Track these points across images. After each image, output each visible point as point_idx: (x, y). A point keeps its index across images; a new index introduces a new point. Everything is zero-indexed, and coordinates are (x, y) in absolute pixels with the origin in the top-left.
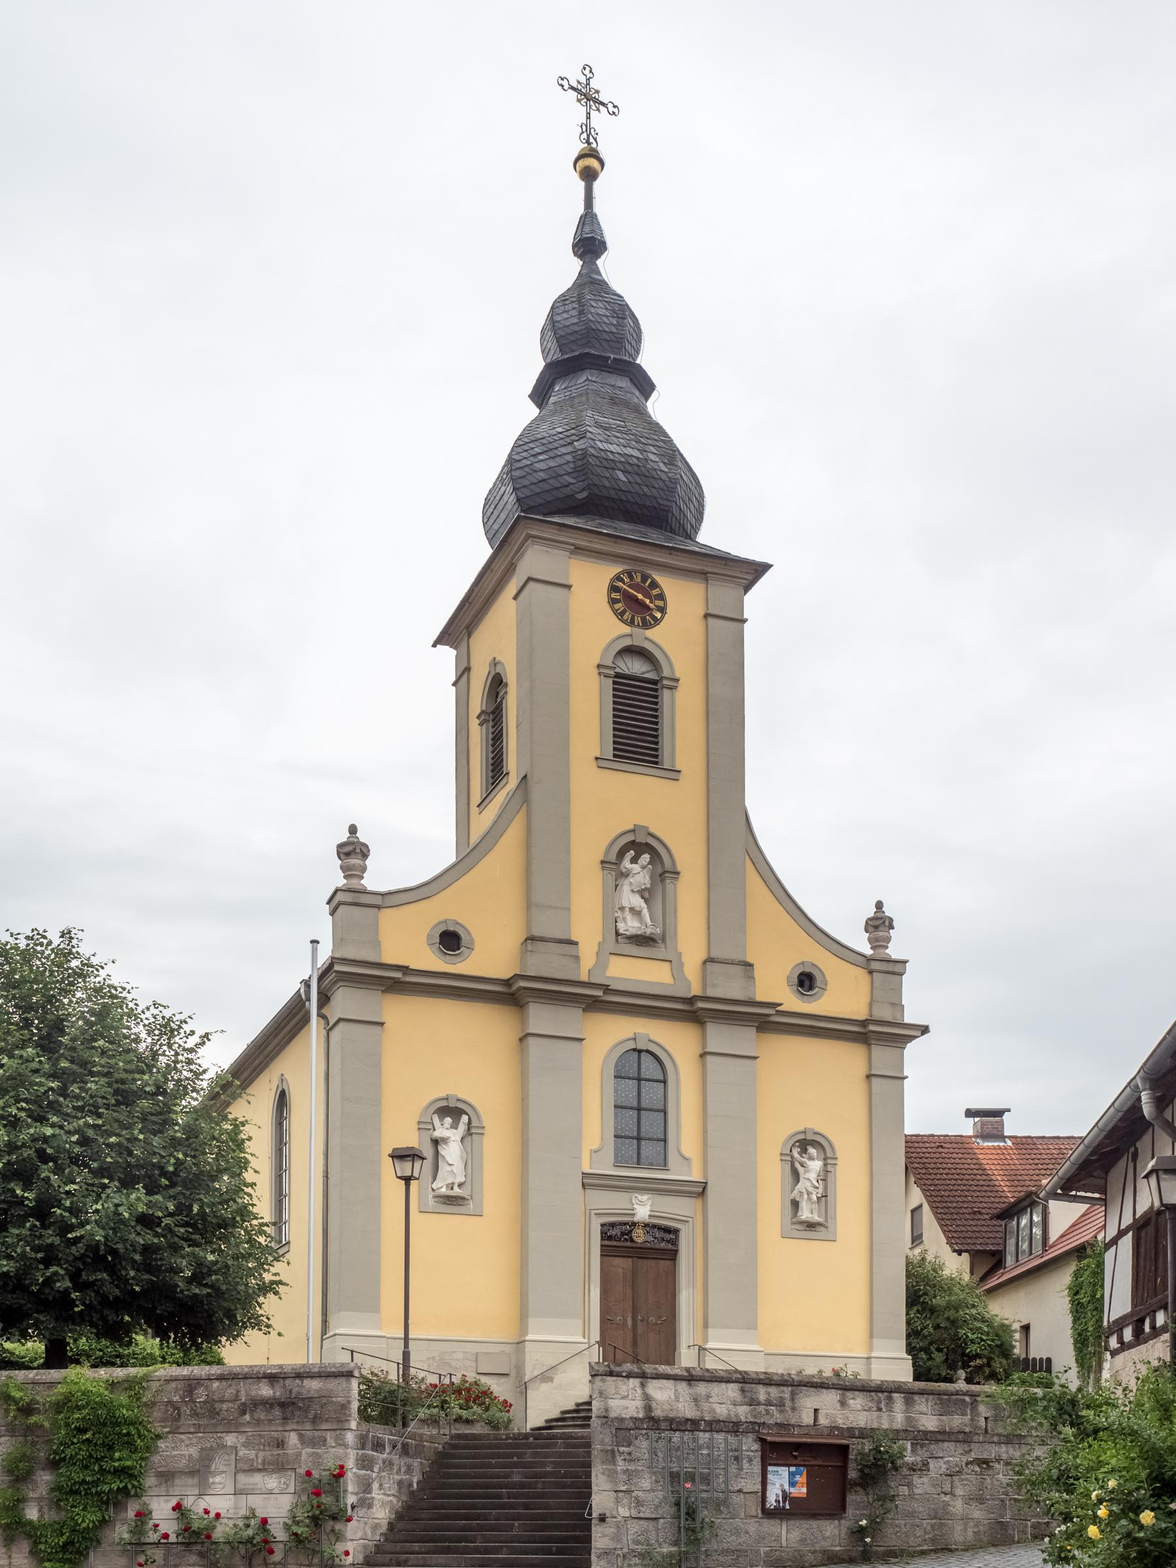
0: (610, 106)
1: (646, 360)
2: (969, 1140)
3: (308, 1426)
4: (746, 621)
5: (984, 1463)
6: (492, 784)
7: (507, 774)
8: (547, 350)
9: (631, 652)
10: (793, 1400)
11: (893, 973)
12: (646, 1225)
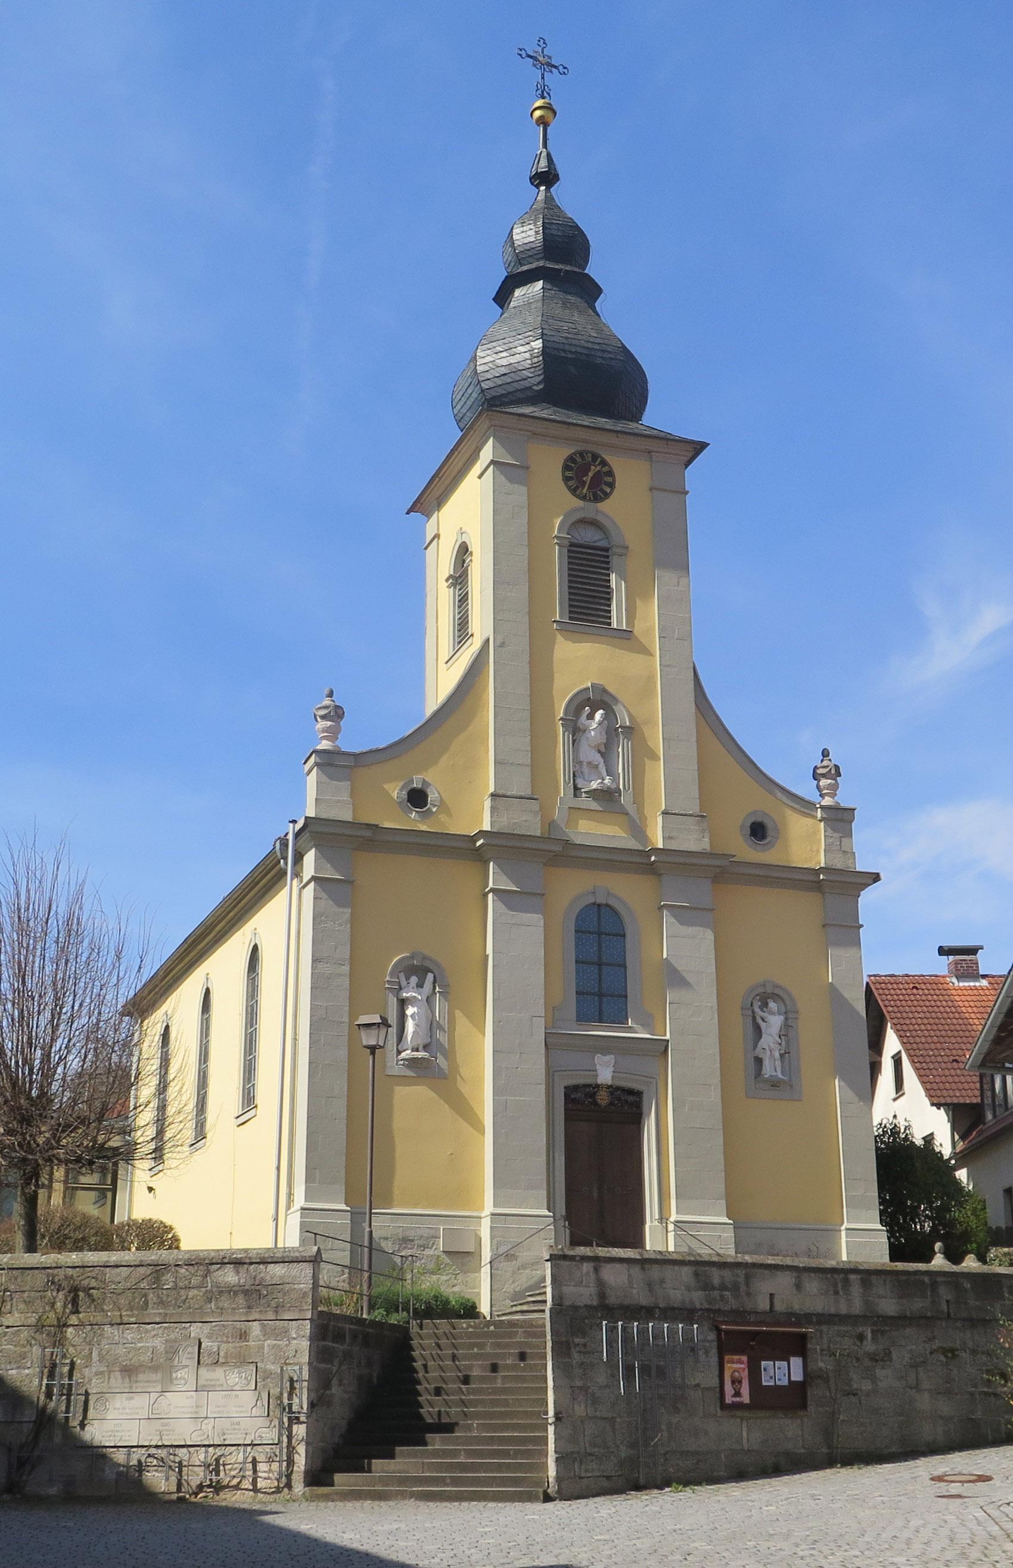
0: (561, 68)
1: (594, 269)
2: (942, 980)
3: (271, 1315)
4: (687, 493)
5: (951, 1353)
6: (459, 642)
7: (472, 635)
8: (508, 262)
9: (583, 521)
10: (747, 1285)
11: (842, 820)
12: (609, 1087)
